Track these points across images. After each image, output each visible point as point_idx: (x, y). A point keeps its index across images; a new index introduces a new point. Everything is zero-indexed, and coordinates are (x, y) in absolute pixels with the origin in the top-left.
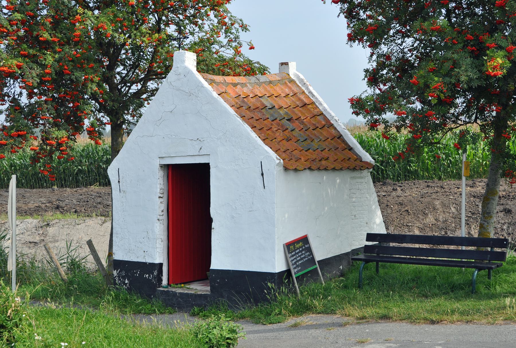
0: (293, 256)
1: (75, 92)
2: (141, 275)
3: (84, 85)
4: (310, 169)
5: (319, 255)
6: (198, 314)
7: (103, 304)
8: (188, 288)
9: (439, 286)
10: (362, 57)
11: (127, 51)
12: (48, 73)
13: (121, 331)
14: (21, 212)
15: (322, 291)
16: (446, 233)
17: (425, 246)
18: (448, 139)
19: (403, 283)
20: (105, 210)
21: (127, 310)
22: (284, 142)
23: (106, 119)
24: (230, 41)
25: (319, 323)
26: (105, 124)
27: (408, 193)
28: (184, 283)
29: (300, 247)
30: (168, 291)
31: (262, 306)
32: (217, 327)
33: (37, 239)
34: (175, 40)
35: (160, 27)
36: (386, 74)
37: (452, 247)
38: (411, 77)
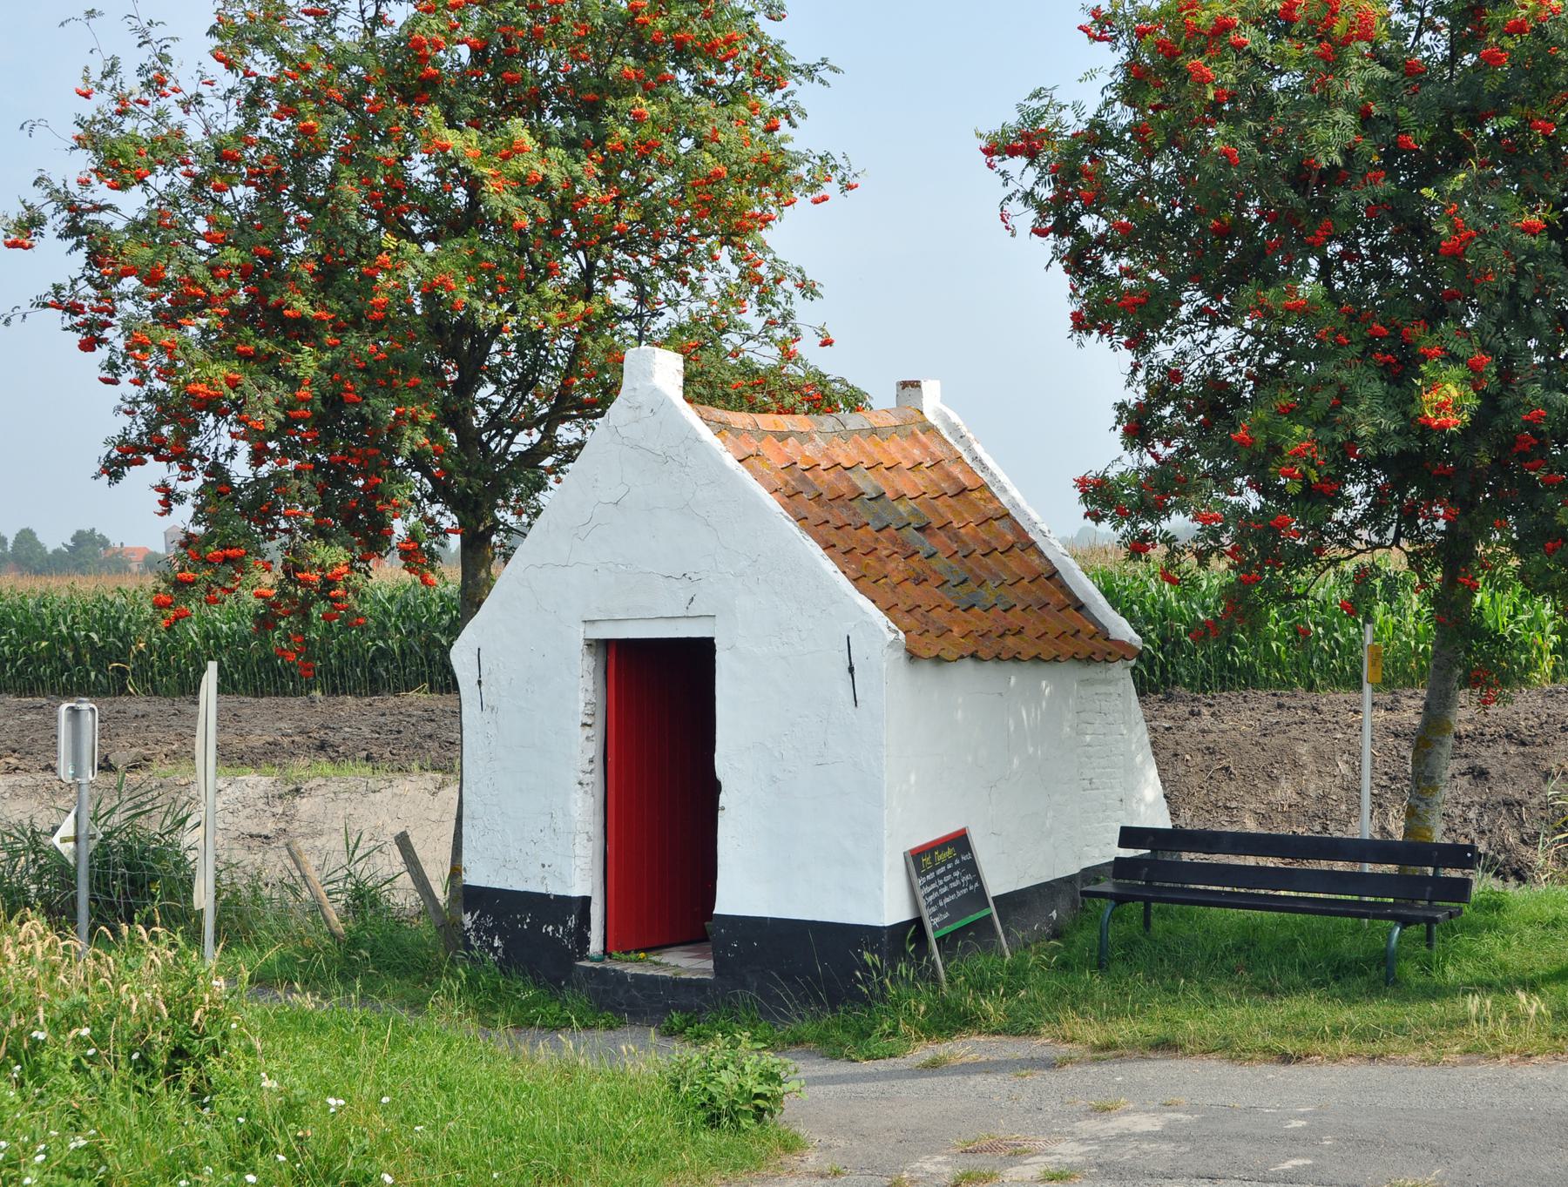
0: (928, 883)
1: (370, 451)
2: (535, 927)
3: (395, 431)
4: (974, 656)
5: (997, 883)
6: (682, 1031)
7: (437, 999)
8: (656, 964)
9: (1303, 966)
10: (1107, 372)
11: (505, 345)
12: (303, 400)
13: (481, 1071)
14: (228, 757)
15: (1004, 975)
16: (1325, 828)
17: (1270, 862)
18: (1327, 587)
19: (1213, 956)
20: (444, 756)
21: (500, 1017)
22: (909, 585)
23: (448, 520)
24: (771, 323)
25: (996, 1058)
26: (446, 533)
27: (1228, 723)
28: (645, 950)
29: (949, 861)
30: (603, 969)
31: (847, 1012)
32: (731, 1067)
33: (270, 827)
34: (629, 318)
35: (590, 286)
36: (1172, 415)
37: (1339, 866)
38: (1234, 426)
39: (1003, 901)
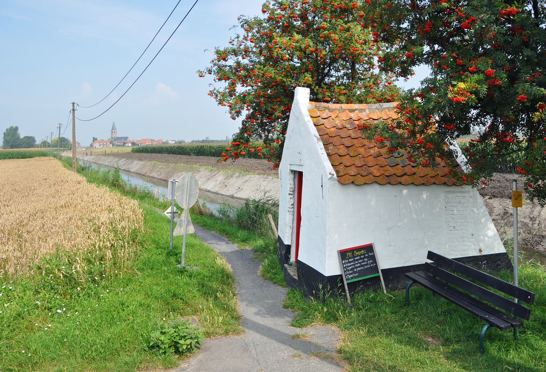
29: (361, 255)
39: (386, 272)
